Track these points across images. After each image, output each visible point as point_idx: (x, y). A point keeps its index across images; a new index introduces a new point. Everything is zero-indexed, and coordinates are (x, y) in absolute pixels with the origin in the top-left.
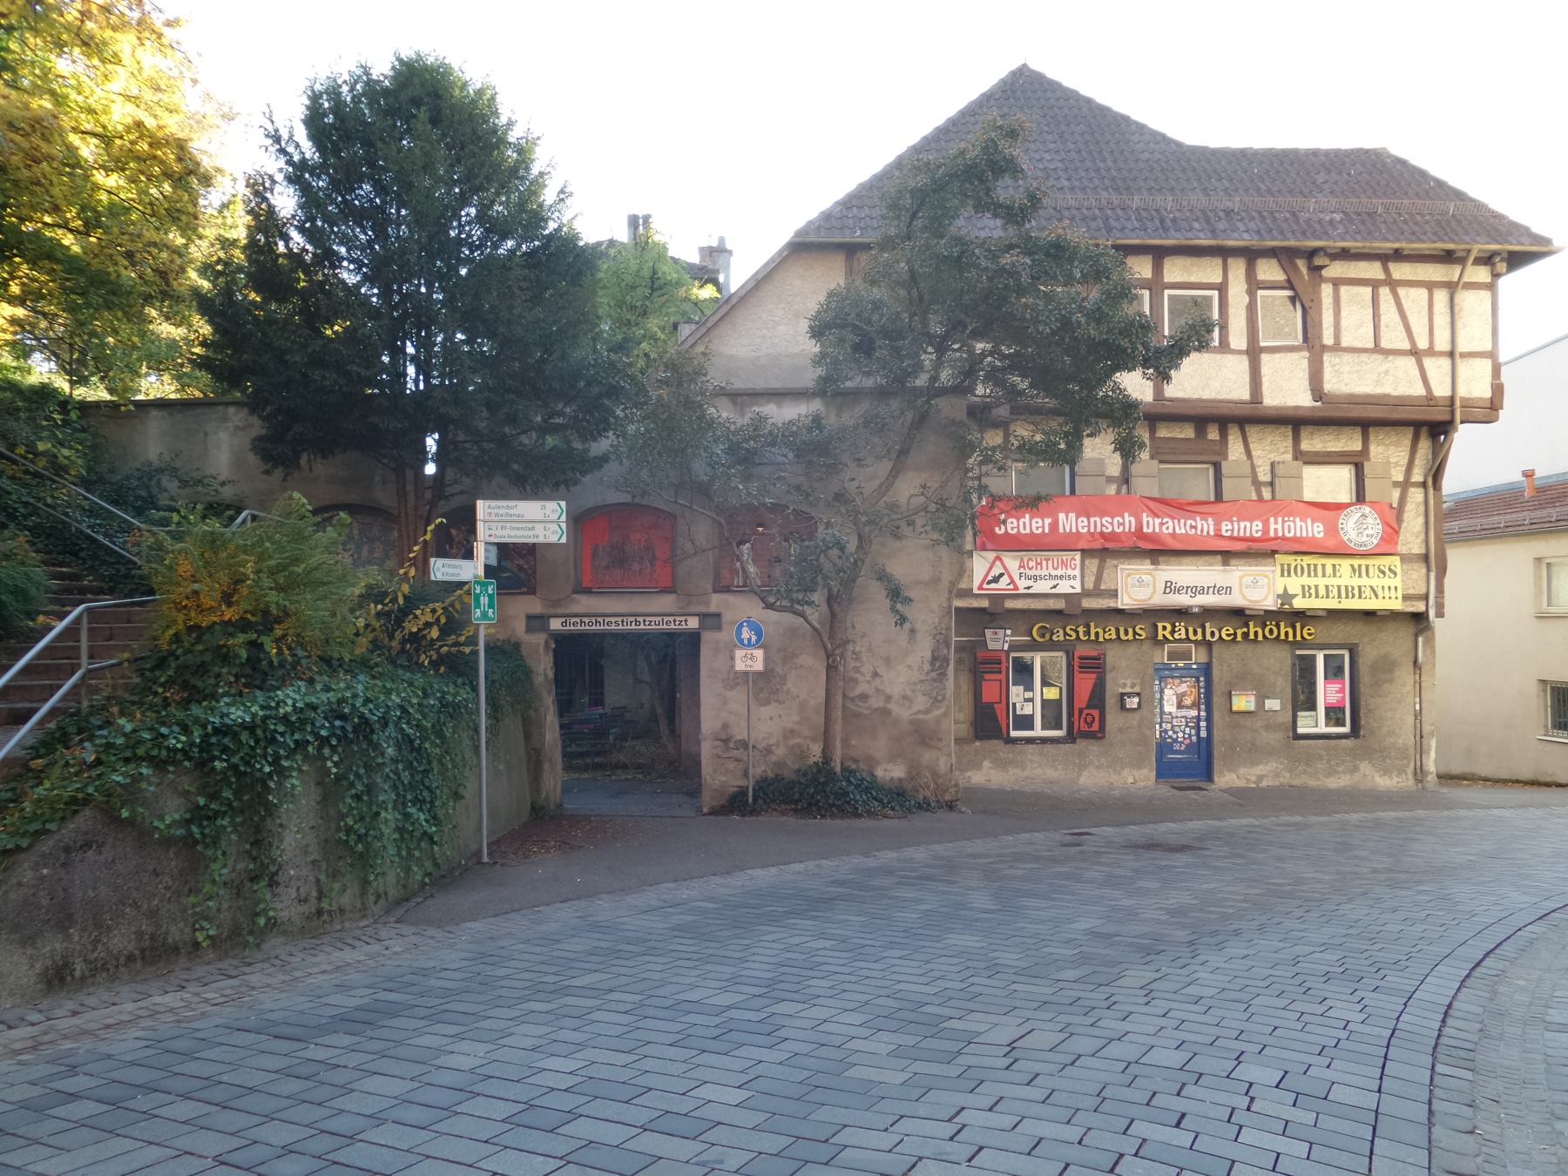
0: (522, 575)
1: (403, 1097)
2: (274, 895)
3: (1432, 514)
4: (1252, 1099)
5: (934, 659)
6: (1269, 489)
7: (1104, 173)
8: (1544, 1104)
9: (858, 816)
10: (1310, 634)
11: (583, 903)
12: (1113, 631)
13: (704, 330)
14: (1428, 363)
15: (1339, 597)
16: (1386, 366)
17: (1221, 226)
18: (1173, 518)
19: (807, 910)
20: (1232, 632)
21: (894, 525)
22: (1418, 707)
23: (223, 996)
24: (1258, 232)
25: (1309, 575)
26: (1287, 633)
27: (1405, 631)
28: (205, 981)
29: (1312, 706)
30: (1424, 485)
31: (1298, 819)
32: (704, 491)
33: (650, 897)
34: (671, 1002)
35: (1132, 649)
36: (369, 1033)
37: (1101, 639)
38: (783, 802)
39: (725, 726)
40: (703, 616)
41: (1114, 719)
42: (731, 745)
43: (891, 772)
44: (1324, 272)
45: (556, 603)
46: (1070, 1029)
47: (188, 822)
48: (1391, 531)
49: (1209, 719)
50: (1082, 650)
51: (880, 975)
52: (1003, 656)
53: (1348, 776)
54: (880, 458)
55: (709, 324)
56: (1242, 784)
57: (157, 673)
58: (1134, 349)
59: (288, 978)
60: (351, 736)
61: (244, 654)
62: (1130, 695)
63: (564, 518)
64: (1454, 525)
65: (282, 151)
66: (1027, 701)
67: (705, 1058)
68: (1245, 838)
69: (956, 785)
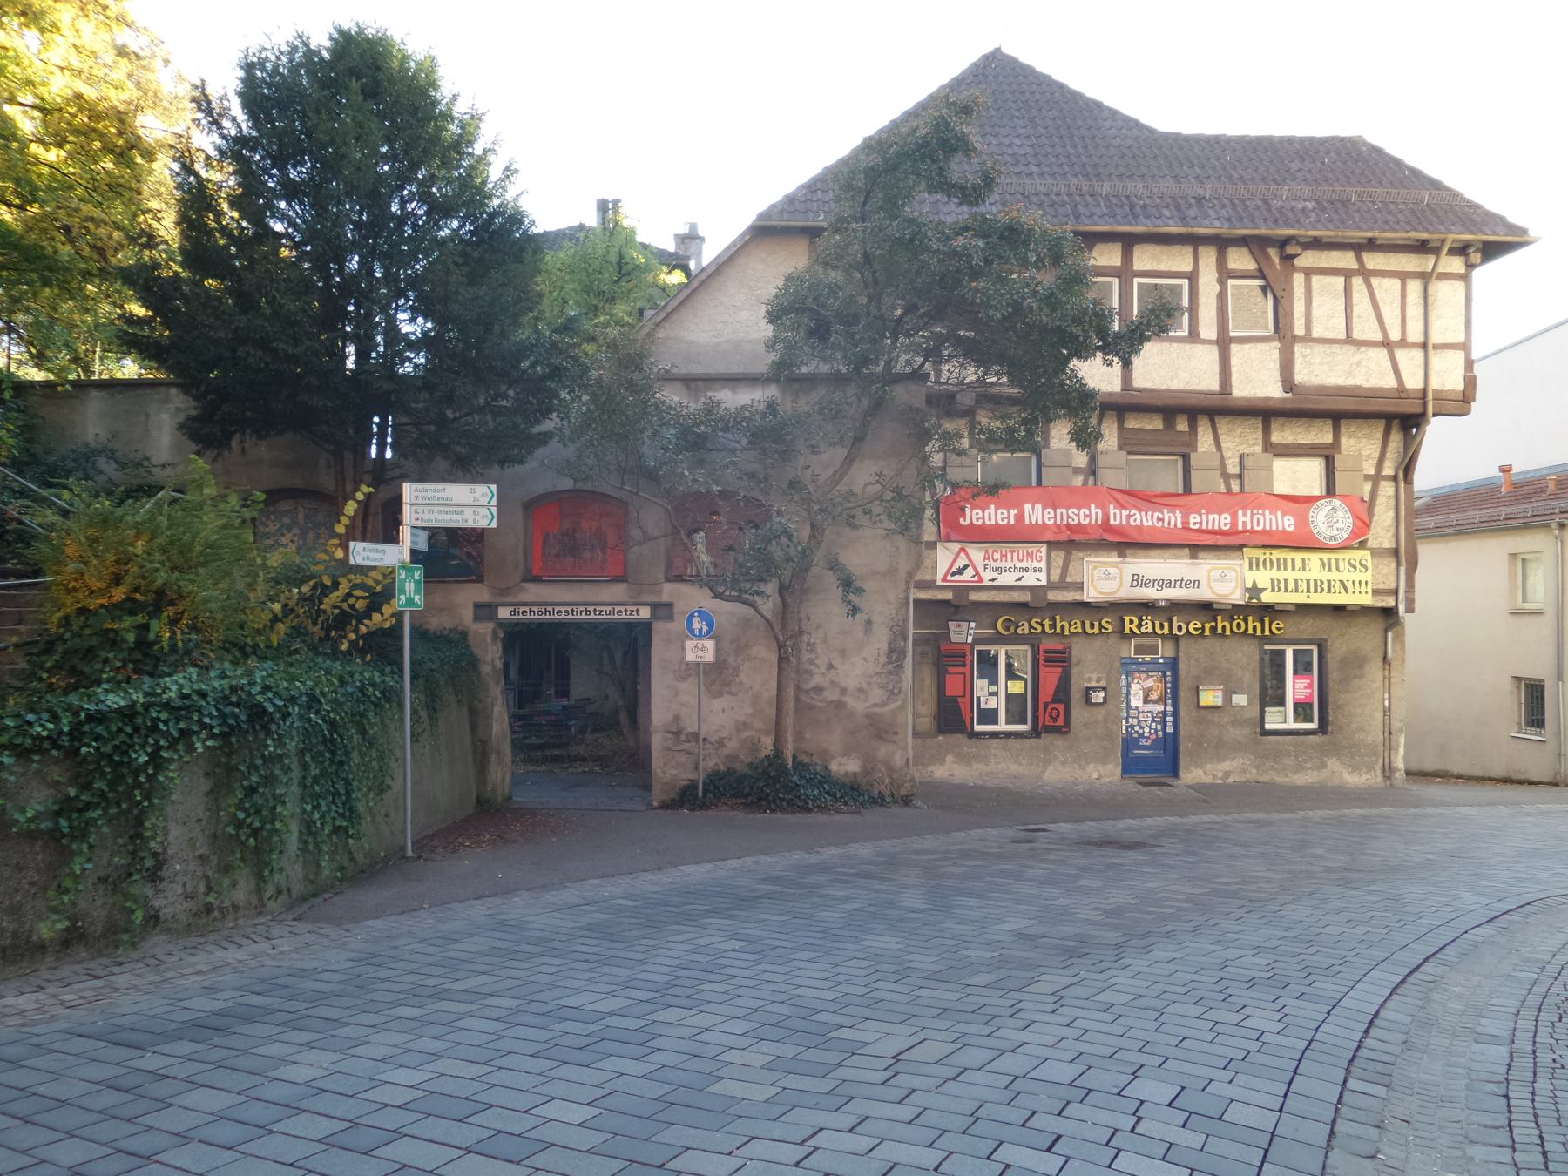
0: (471, 563)
1: (220, 1114)
2: (158, 891)
3: (1403, 508)
4: (1139, 1119)
5: (891, 651)
6: (1238, 481)
7: (1074, 159)
8: (1458, 1125)
9: (809, 811)
10: (1278, 629)
11: (497, 901)
12: (1079, 625)
13: (663, 315)
14: (1400, 354)
15: (1308, 591)
16: (1358, 357)
17: (1192, 213)
18: (1140, 510)
19: (729, 909)
20: (1199, 626)
21: (849, 514)
22: (1387, 703)
23: (82, 998)
24: (1229, 220)
25: (1279, 569)
26: (1255, 627)
27: (1375, 626)
28: (68, 981)
29: (1281, 702)
30: (1395, 478)
31: (1261, 815)
32: (652, 476)
33: (571, 894)
34: (550, 1007)
35: (1099, 642)
36: (216, 1040)
37: (1067, 633)
38: (734, 796)
39: (677, 718)
40: (655, 607)
41: (1079, 714)
42: (683, 737)
43: (845, 766)
44: (1297, 262)
45: (506, 591)
46: (965, 1040)
47: (58, 814)
48: (1361, 524)
49: (1175, 714)
50: (1047, 644)
51: (781, 978)
52: (968, 649)
53: (1315, 773)
54: (834, 445)
55: (669, 309)
56: (1209, 780)
57: (44, 658)
58: (1087, 337)
59: (158, 978)
60: (245, 726)
61: (131, 638)
62: (1095, 689)
63: (494, 502)
64: (1431, 521)
65: (216, 123)
66: (992, 694)
67: (564, 1071)
68: (1202, 835)
69: (912, 780)
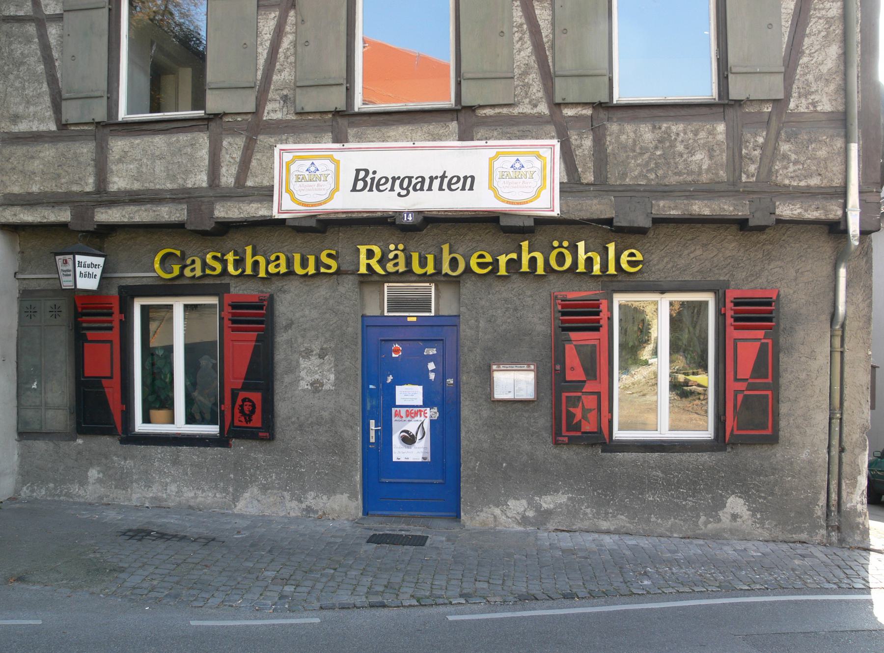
12: (283, 261)
20: (489, 259)
26: (589, 261)
37: (262, 274)
50: (240, 291)
